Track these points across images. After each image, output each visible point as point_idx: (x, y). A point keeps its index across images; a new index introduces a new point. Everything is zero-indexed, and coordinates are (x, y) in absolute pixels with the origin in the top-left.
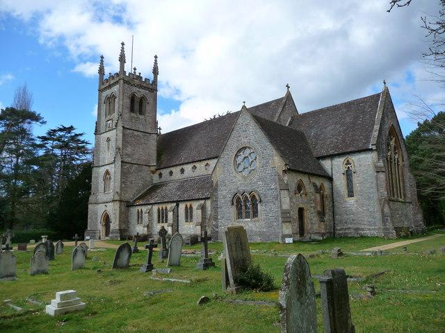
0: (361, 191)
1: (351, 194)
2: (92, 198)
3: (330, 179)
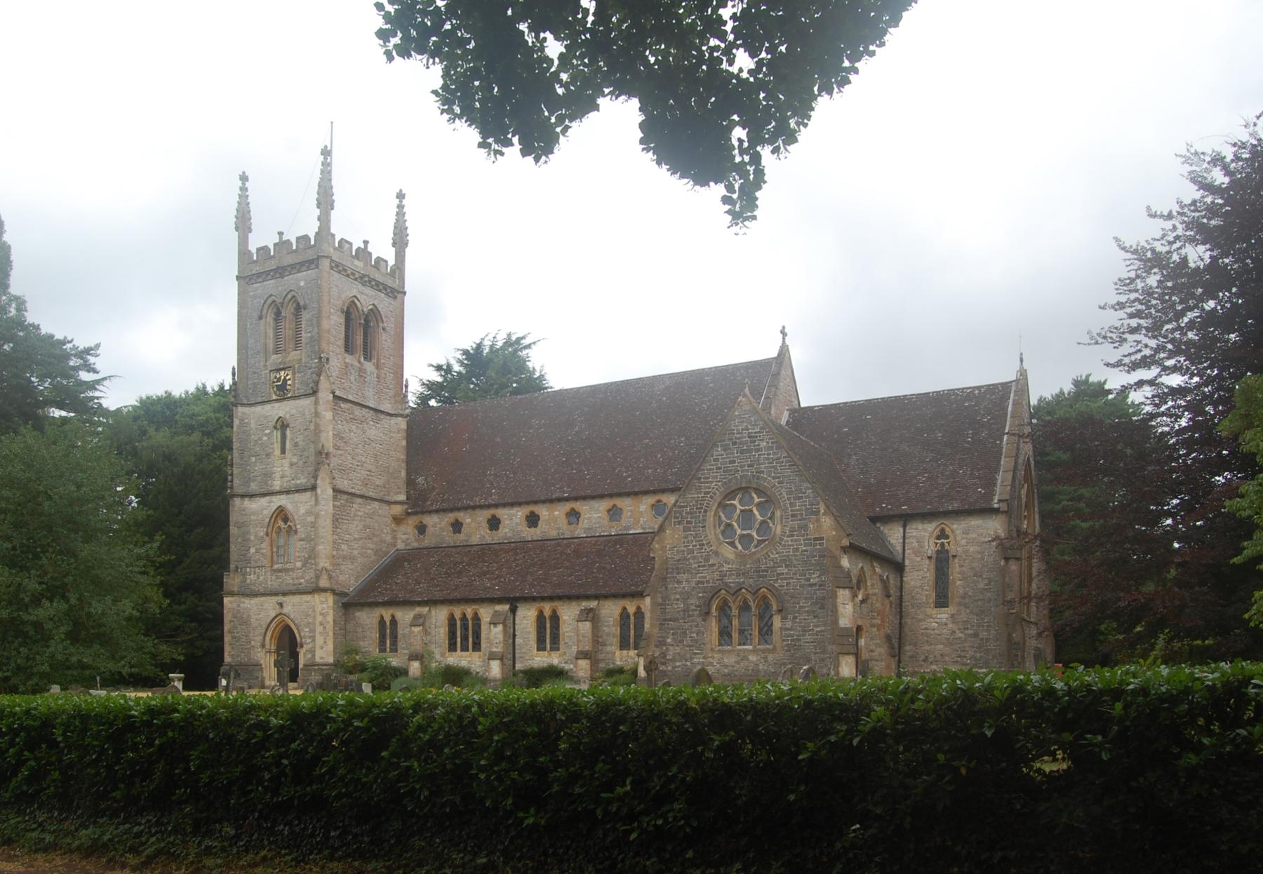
0: (963, 597)
2: (231, 581)
3: (898, 567)
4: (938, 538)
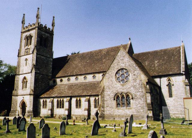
0: (176, 94)
1: (171, 95)
4: (168, 81)
